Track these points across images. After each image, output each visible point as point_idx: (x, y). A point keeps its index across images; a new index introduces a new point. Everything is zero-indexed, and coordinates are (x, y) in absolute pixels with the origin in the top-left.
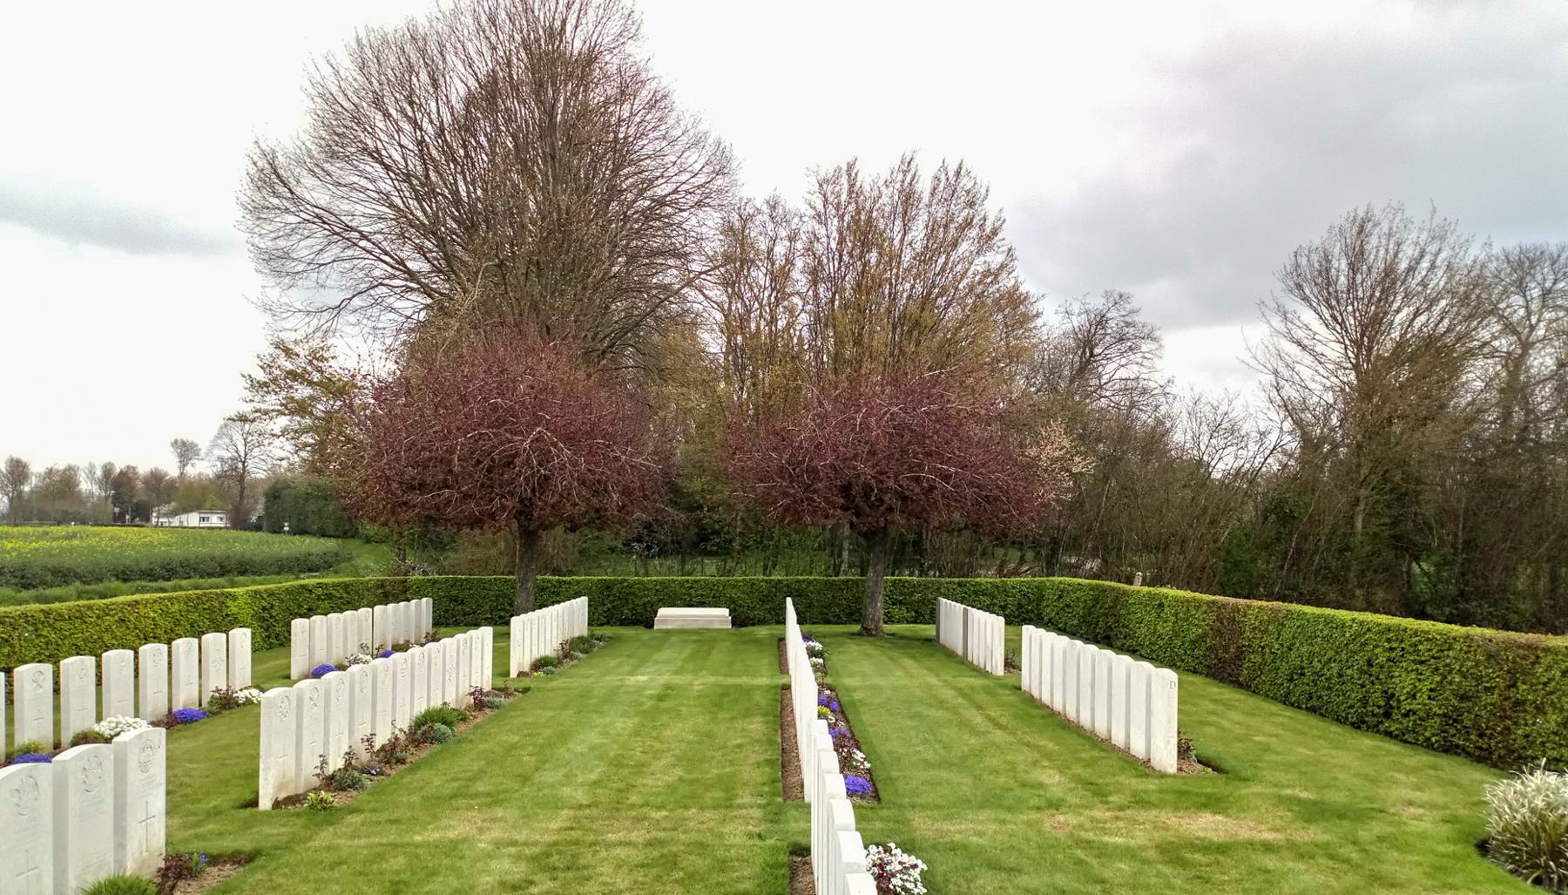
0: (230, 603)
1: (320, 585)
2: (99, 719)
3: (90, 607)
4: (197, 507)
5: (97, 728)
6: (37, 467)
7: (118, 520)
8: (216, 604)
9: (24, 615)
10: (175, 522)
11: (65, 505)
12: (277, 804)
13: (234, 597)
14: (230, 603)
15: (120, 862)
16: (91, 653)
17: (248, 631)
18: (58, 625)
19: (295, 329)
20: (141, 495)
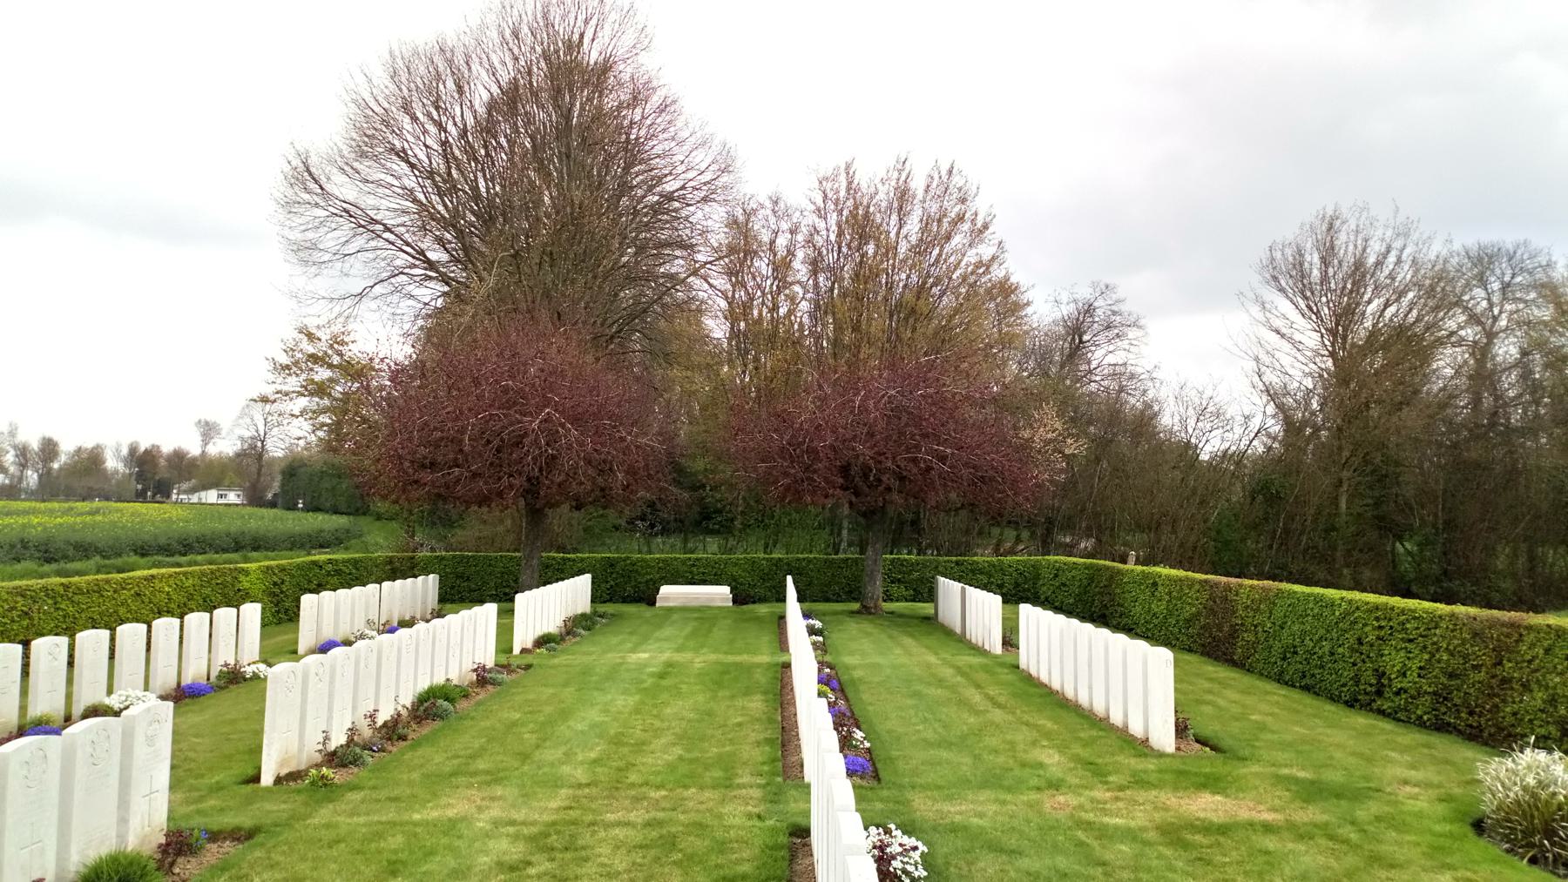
0: (242, 578)
1: (330, 561)
2: (110, 692)
3: (107, 582)
5: (107, 701)
6: (67, 446)
7: (140, 496)
9: (45, 589)
10: (195, 498)
12: (278, 780)
13: (246, 572)
14: (242, 578)
15: (122, 837)
17: (258, 607)
18: (76, 598)
19: (319, 316)
20: (163, 472)
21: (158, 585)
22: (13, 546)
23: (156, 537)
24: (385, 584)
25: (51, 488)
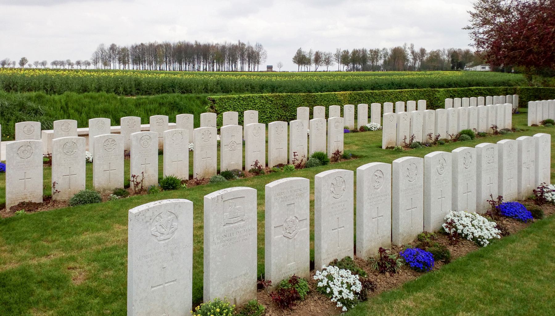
0: (437, 93)
1: (477, 89)
2: (369, 121)
3: (386, 92)
4: (481, 63)
6: (428, 51)
7: (452, 69)
8: (431, 93)
9: (365, 93)
11: (435, 64)
12: (387, 148)
13: (439, 92)
14: (437, 93)
16: (191, 112)
18: (375, 97)
21: (403, 94)
22: (389, 85)
23: (439, 81)
24: (494, 97)
25: (424, 67)
